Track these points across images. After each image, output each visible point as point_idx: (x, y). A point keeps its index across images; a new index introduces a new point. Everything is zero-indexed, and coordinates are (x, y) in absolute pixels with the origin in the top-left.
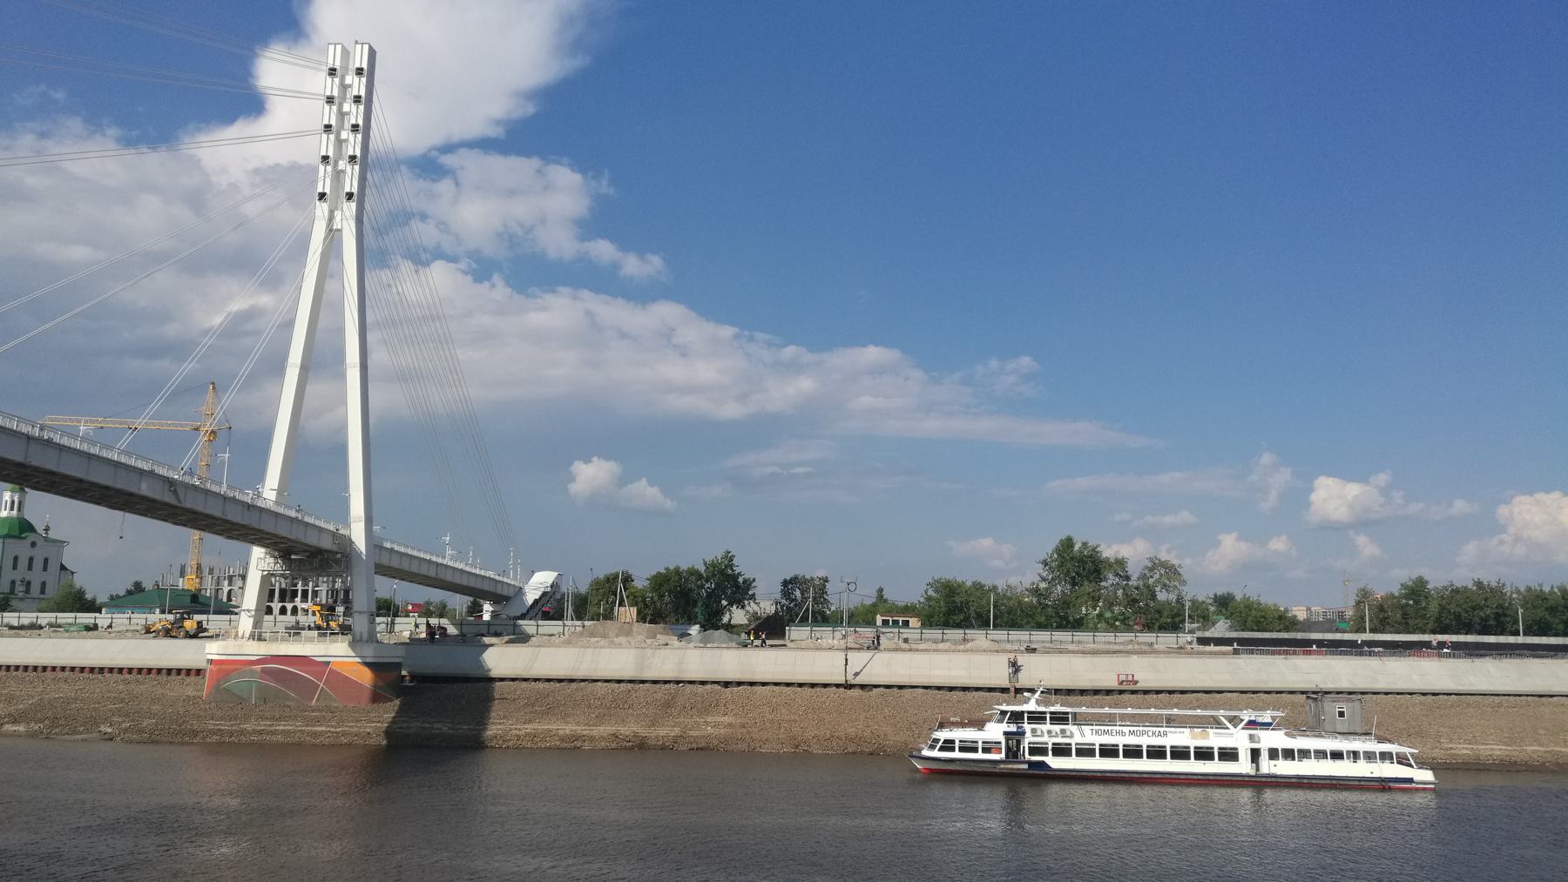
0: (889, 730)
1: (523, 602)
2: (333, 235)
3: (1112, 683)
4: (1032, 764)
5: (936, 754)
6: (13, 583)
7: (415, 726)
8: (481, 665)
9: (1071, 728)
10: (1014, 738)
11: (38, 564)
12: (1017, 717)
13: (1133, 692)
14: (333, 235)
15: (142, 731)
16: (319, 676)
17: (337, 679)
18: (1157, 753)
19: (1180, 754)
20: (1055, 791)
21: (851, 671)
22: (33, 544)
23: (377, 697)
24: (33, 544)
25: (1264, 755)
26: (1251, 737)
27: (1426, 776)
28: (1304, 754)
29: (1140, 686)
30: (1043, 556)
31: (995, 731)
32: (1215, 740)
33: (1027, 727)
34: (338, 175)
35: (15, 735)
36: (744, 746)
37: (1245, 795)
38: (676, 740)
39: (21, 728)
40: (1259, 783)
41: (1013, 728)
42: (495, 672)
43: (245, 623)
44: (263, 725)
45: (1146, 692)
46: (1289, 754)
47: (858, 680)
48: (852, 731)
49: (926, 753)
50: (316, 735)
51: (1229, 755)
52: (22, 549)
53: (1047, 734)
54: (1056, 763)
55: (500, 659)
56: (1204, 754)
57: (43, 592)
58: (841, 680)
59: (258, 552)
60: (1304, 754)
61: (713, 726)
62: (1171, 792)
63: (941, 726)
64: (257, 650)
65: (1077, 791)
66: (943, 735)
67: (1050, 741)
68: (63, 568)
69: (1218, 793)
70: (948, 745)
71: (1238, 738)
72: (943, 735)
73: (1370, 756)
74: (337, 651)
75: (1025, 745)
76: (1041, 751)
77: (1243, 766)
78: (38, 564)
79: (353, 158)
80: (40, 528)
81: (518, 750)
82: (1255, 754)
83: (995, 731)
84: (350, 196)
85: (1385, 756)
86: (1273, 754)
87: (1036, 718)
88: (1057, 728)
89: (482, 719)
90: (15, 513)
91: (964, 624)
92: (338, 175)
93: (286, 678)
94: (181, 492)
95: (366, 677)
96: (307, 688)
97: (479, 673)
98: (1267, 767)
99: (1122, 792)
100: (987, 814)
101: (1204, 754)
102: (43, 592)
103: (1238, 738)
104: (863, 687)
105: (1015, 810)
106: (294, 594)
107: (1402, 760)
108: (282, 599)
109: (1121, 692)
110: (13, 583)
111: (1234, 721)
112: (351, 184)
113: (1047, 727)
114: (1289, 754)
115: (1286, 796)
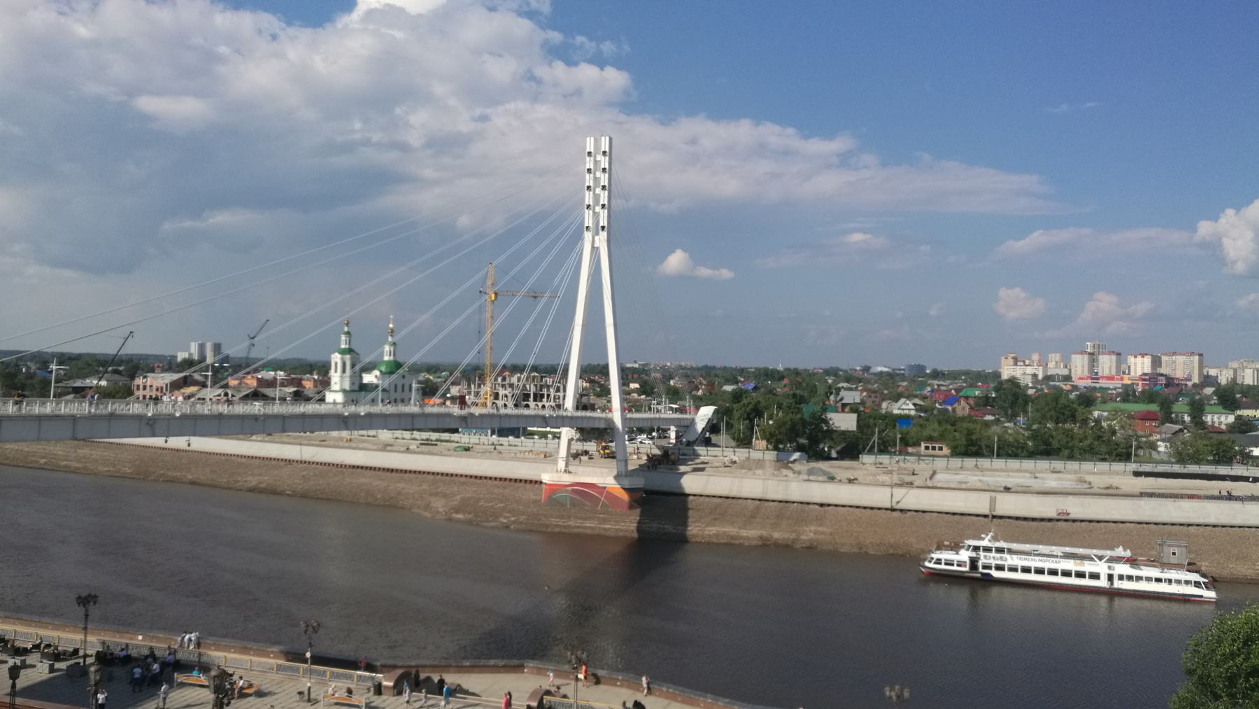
0: (913, 540)
1: (695, 430)
2: (595, 250)
3: (1053, 514)
4: (983, 574)
5: (931, 565)
7: (655, 526)
8: (680, 486)
9: (1006, 555)
10: (974, 563)
12: (976, 549)
13: (1066, 520)
14: (595, 250)
15: (521, 523)
16: (601, 494)
17: (610, 496)
18: (1053, 572)
19: (1067, 574)
20: (995, 591)
21: (895, 500)
23: (631, 507)
25: (1116, 578)
26: (1109, 568)
27: (1210, 594)
28: (1139, 578)
29: (1071, 517)
31: (964, 555)
32: (1087, 567)
33: (982, 554)
34: (596, 215)
35: (458, 521)
36: (830, 547)
37: (1103, 601)
38: (794, 541)
39: (460, 516)
40: (1112, 594)
41: (974, 555)
42: (688, 490)
43: (561, 465)
44: (579, 522)
45: (1074, 521)
46: (1130, 578)
47: (900, 506)
48: (892, 541)
49: (927, 564)
50: (606, 529)
51: (1095, 576)
53: (992, 559)
54: (996, 574)
55: (691, 483)
56: (1080, 575)
58: (888, 506)
60: (1139, 578)
61: (809, 533)
62: (1057, 595)
63: (940, 547)
64: (567, 479)
65: (1008, 592)
66: (936, 556)
67: (993, 563)
69: (1088, 599)
70: (939, 562)
71: (1102, 568)
72: (936, 556)
73: (1178, 582)
74: (603, 476)
75: (980, 564)
76: (989, 567)
77: (1103, 583)
81: (710, 546)
82: (1110, 577)
83: (964, 555)
84: (603, 228)
85: (1187, 582)
86: (1121, 577)
87: (987, 549)
88: (998, 555)
89: (685, 524)
91: (977, 454)
92: (596, 215)
93: (585, 494)
95: (625, 497)
96: (594, 500)
97: (678, 491)
98: (1118, 584)
99: (1032, 594)
100: (960, 596)
101: (1080, 575)
103: (1102, 568)
104: (901, 510)
105: (973, 595)
106: (542, 396)
107: (1197, 584)
108: (535, 400)
109: (1058, 520)
111: (1100, 558)
112: (603, 221)
113: (993, 554)
114: (1130, 578)
115: (1128, 603)
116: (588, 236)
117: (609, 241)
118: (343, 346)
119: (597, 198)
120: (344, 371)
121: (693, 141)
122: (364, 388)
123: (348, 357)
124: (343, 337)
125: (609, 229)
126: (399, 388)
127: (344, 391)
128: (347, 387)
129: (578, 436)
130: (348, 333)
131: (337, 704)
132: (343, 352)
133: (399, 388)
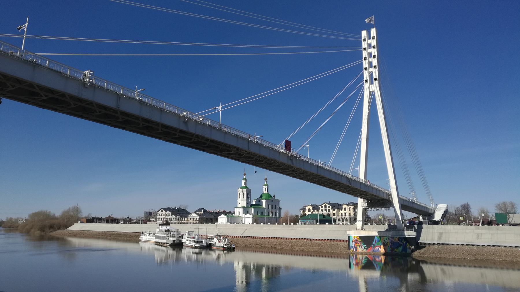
2: (372, 94)
11: (274, 207)
14: (372, 94)
30: (280, 202)
43: (359, 224)
78: (274, 207)
84: (376, 79)
92: (371, 75)
112: (376, 75)
116: (366, 85)
119: (370, 64)
120: (243, 197)
123: (245, 190)
127: (244, 207)
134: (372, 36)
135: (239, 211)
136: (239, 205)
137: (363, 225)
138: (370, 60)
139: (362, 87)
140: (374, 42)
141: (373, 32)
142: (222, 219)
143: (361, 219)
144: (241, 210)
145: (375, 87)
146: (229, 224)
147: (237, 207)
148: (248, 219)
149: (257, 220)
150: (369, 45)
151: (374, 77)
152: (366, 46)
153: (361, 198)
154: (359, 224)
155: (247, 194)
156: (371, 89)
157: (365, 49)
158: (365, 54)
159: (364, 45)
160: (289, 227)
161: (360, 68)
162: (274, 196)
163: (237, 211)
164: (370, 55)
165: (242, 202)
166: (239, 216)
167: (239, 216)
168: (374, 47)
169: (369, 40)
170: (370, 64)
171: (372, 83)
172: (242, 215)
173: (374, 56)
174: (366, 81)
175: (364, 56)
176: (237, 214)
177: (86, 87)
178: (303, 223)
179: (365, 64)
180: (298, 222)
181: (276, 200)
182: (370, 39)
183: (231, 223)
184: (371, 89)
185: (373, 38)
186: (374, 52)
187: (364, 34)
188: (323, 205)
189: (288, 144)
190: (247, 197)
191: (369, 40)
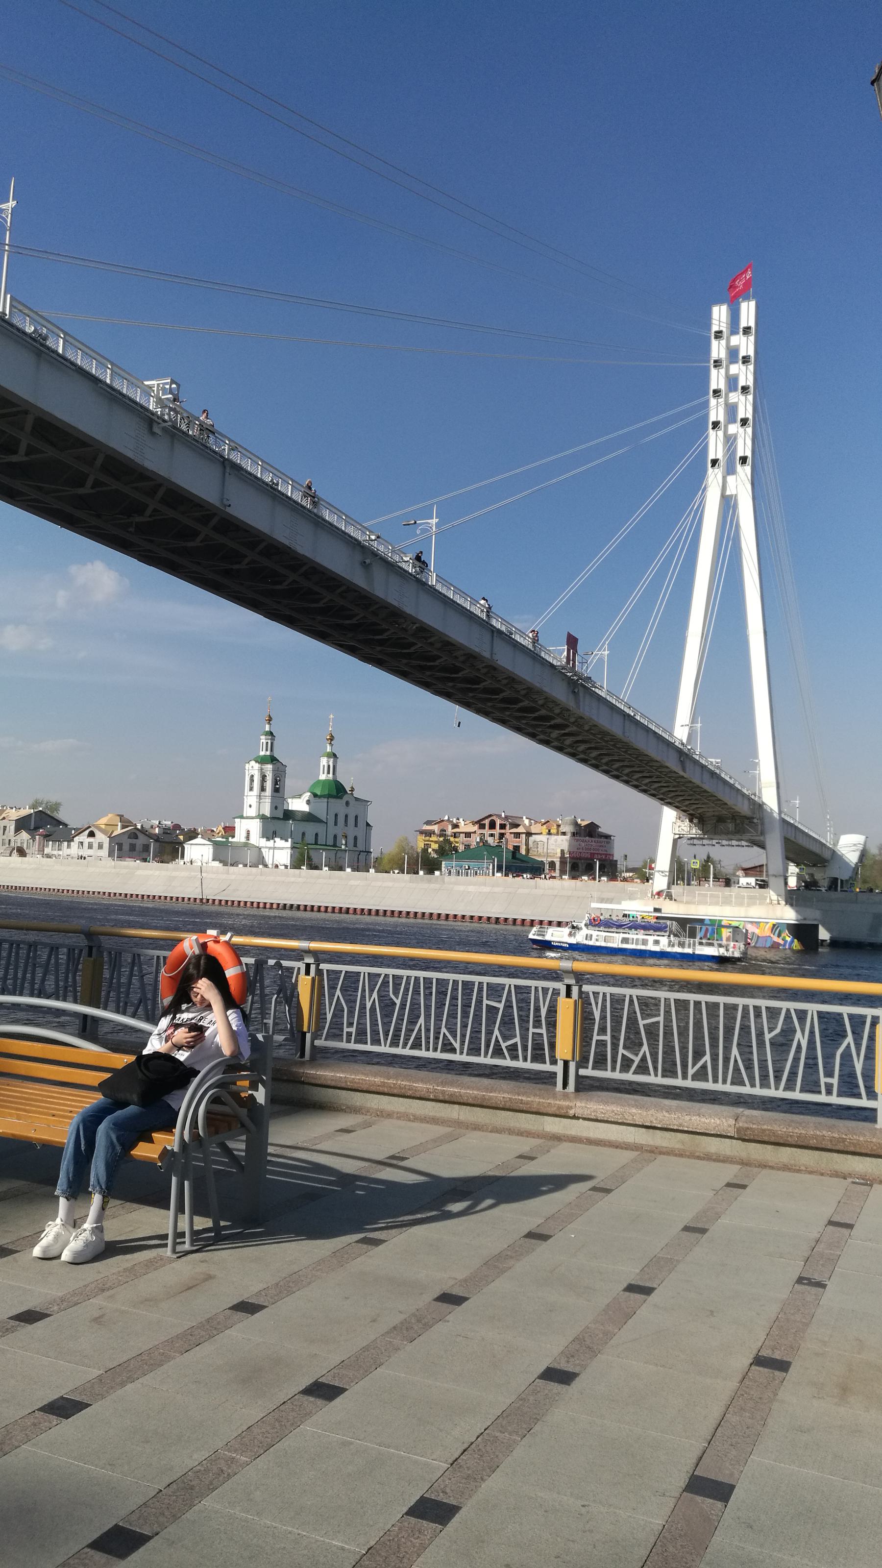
2: (728, 504)
6: (335, 837)
11: (351, 821)
14: (728, 504)
22: (347, 803)
24: (347, 803)
30: (370, 808)
34: (730, 441)
43: (660, 882)
52: (338, 806)
57: (355, 845)
59: (669, 814)
68: (368, 825)
78: (351, 821)
79: (744, 422)
80: (348, 789)
84: (744, 460)
90: (331, 775)
92: (730, 441)
94: (688, 765)
102: (355, 845)
110: (335, 837)
112: (744, 448)
116: (714, 477)
117: (754, 483)
118: (262, 753)
119: (731, 410)
120: (263, 789)
121: (570, 934)
122: (289, 815)
123: (269, 767)
124: (263, 739)
125: (757, 463)
126: (341, 820)
127: (263, 818)
128: (268, 813)
129: (695, 831)
130: (271, 733)
131: (729, 1185)
132: (262, 761)
133: (341, 820)
134: (743, 324)
135: (249, 829)
136: (251, 812)
137: (671, 883)
138: (733, 429)
139: (694, 482)
140: (746, 345)
141: (748, 312)
142: (198, 851)
143: (667, 868)
144: (255, 826)
145: (740, 485)
146: (216, 864)
147: (242, 817)
148: (280, 852)
149: (303, 859)
150: (733, 354)
151: (740, 453)
152: (723, 355)
153: (669, 804)
154: (660, 882)
155: (276, 782)
156: (729, 490)
157: (717, 363)
158: (717, 379)
159: (718, 350)
160: (429, 881)
161: (700, 426)
162: (352, 790)
163: (241, 827)
164: (732, 382)
165: (254, 803)
166: (246, 845)
167: (246, 845)
168: (746, 360)
169: (733, 333)
170: (731, 410)
171: (730, 470)
172: (256, 839)
173: (745, 389)
174: (714, 462)
175: (713, 386)
176: (239, 837)
177: (153, 434)
178: (453, 871)
179: (716, 411)
180: (440, 869)
181: (357, 799)
182: (734, 331)
183: (225, 864)
184: (729, 490)
185: (747, 331)
186: (746, 375)
187: (720, 315)
188: (487, 822)
189: (572, 642)
190: (276, 790)
191: (733, 333)
